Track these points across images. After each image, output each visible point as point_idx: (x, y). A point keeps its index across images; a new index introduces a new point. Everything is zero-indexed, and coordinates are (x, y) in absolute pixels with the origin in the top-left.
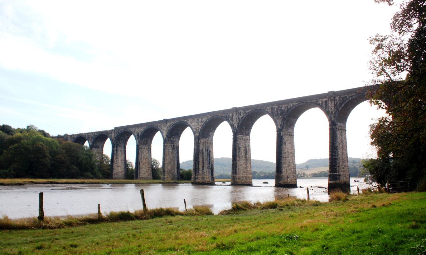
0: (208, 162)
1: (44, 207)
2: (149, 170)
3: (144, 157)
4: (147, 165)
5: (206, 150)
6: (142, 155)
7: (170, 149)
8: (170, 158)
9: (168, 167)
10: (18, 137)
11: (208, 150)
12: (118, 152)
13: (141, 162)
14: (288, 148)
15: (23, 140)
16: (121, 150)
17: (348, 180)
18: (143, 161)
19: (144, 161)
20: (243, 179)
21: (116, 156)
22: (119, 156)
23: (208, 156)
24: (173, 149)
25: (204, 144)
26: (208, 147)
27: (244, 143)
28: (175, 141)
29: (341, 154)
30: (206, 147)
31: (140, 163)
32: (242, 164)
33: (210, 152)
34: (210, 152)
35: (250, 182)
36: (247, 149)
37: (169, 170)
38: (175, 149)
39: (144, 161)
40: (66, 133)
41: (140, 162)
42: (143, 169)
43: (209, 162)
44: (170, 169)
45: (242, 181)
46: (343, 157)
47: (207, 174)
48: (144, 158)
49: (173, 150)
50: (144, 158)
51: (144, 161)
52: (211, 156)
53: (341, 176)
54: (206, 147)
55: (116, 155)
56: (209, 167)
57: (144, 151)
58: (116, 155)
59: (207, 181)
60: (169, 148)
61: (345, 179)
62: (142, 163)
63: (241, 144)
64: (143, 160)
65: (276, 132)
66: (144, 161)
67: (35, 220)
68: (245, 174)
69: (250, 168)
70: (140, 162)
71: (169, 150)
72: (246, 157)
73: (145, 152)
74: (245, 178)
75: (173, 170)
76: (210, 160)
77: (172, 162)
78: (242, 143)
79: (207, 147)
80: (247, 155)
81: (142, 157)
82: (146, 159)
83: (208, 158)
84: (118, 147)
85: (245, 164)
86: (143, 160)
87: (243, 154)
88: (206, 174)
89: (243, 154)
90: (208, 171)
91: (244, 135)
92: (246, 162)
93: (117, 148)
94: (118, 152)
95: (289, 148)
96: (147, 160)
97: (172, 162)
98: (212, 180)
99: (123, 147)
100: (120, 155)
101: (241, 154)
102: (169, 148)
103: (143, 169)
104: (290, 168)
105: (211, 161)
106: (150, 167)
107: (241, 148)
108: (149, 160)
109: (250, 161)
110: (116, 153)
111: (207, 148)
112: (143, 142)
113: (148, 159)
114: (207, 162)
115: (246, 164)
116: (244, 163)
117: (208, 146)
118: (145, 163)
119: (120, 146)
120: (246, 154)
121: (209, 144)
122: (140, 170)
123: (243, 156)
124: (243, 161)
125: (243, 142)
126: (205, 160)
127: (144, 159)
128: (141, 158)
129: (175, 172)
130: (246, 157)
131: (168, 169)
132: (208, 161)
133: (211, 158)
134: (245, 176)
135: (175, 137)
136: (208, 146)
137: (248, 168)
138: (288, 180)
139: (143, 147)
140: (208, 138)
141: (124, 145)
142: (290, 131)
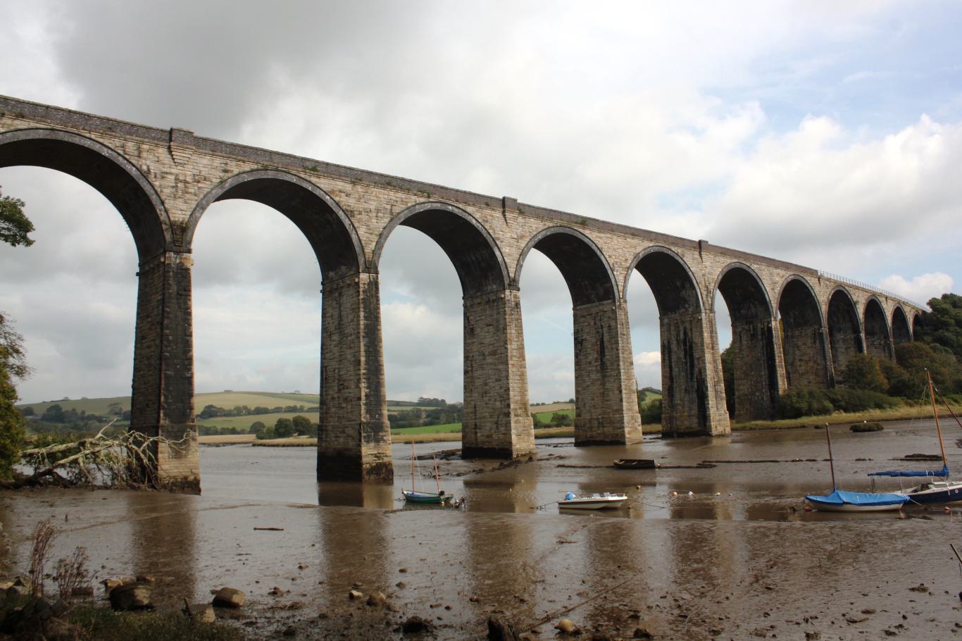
0: (687, 375)
1: (676, 466)
3: (802, 358)
5: (678, 344)
6: (794, 354)
7: (744, 338)
8: (746, 364)
9: (741, 387)
10: (28, 408)
11: (685, 340)
12: (837, 346)
13: (795, 372)
14: (482, 341)
15: (946, 316)
16: (844, 341)
17: (351, 444)
18: (798, 368)
19: (802, 369)
20: (591, 428)
23: (685, 358)
24: (753, 336)
25: (672, 328)
26: (685, 333)
27: (595, 324)
30: (678, 335)
32: (588, 386)
33: (691, 347)
34: (694, 346)
35: (617, 435)
36: (606, 338)
37: (746, 395)
38: (760, 337)
39: (803, 367)
40: (84, 396)
43: (692, 374)
44: (747, 392)
45: (589, 434)
46: (342, 373)
47: (686, 409)
49: (752, 340)
50: (801, 360)
52: (696, 355)
53: (326, 431)
54: (678, 335)
56: (692, 387)
57: (800, 343)
59: (683, 427)
60: (740, 337)
61: (341, 440)
63: (586, 330)
64: (800, 366)
65: (133, 361)
66: (803, 367)
67: (191, 478)
68: (599, 411)
69: (617, 392)
71: (741, 342)
72: (603, 363)
73: (805, 344)
74: (599, 423)
75: (757, 394)
76: (692, 366)
77: (753, 373)
78: (589, 325)
79: (682, 333)
80: (607, 357)
81: (794, 359)
82: (807, 362)
83: (686, 363)
85: (601, 384)
86: (800, 366)
87: (591, 357)
88: (683, 407)
89: (591, 357)
90: (686, 399)
91: (594, 302)
92: (604, 377)
94: (837, 346)
95: (487, 341)
96: (811, 364)
97: (751, 371)
98: (699, 423)
100: (843, 350)
101: (587, 358)
102: (740, 337)
104: (486, 399)
105: (696, 370)
107: (586, 340)
108: (818, 364)
109: (614, 373)
111: (682, 336)
112: (792, 320)
113: (815, 362)
114: (683, 374)
115: (603, 384)
116: (597, 380)
117: (685, 329)
118: (807, 372)
119: (839, 330)
120: (602, 352)
121: (688, 325)
123: (593, 362)
124: (594, 376)
125: (592, 323)
126: (675, 370)
129: (763, 398)
130: (603, 363)
131: (741, 392)
132: (686, 370)
133: (696, 362)
134: (598, 419)
135: (751, 305)
136: (685, 329)
137: (611, 393)
138: (479, 435)
139: (797, 333)
140: (684, 308)
142: (489, 288)
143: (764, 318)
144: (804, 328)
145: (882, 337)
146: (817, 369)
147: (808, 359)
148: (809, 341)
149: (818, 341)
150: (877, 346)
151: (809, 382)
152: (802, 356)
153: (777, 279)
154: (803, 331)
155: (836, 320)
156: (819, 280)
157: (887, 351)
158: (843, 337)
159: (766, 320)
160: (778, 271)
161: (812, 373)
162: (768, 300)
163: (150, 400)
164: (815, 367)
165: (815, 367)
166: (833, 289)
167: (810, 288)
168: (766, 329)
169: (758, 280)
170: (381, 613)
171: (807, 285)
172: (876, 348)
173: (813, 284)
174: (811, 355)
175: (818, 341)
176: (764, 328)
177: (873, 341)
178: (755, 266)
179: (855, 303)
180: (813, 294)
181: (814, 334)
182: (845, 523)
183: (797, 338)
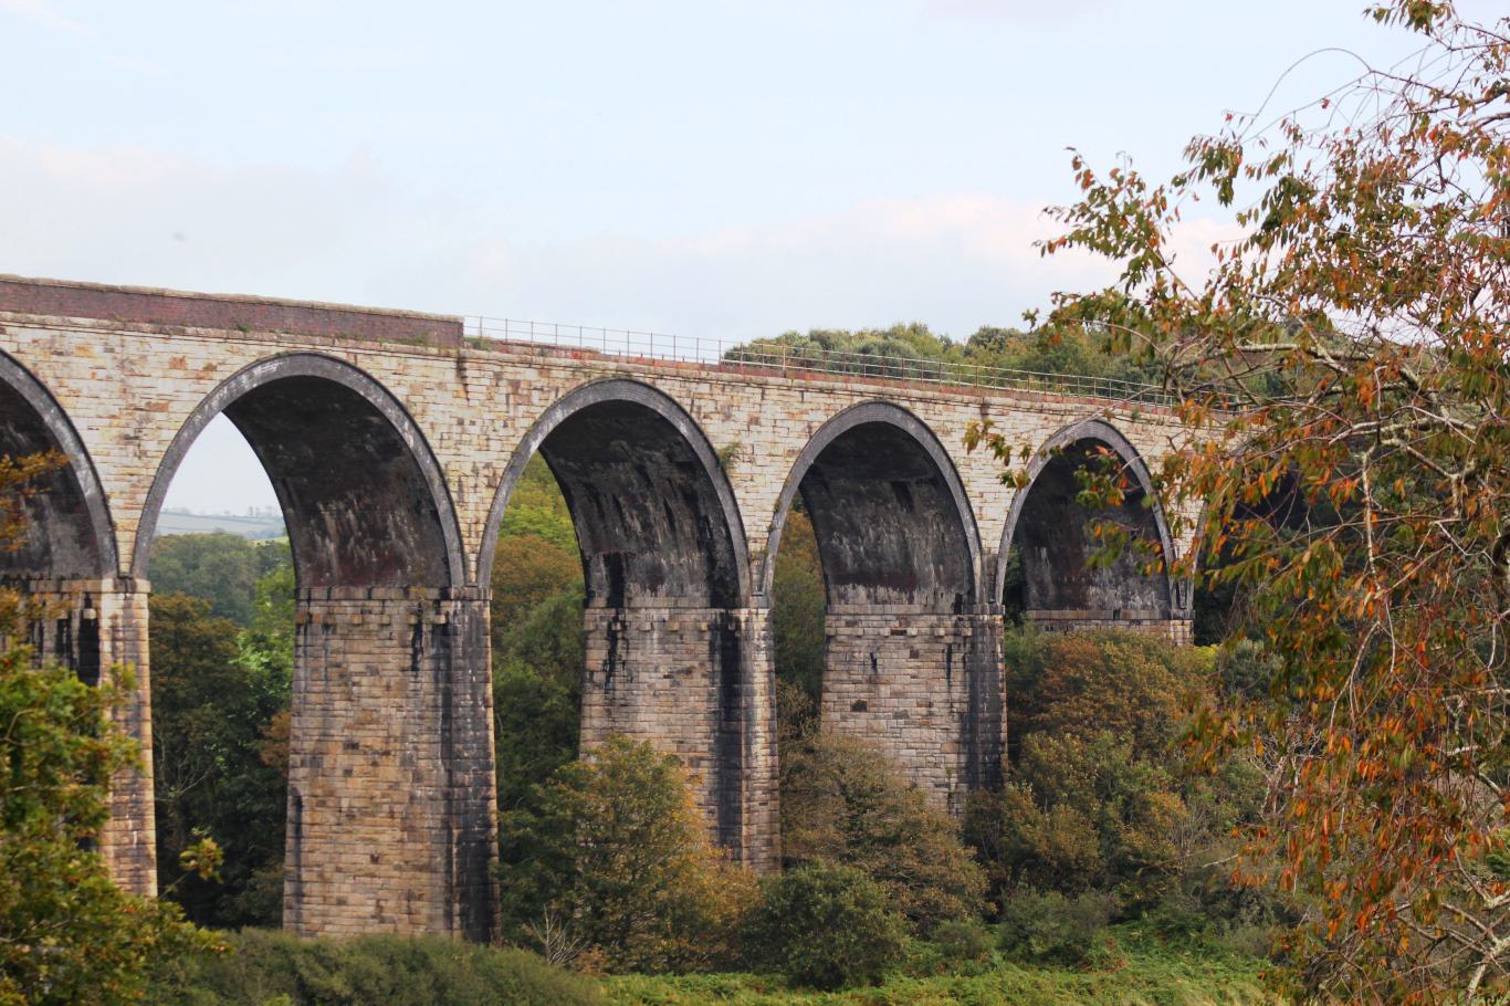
2: (410, 897)
4: (388, 836)
12: (635, 656)
16: (670, 635)
19: (351, 792)
21: (612, 705)
22: (642, 700)
28: (47, 550)
29: (259, 529)
31: (306, 817)
39: (357, 783)
41: (304, 791)
42: (343, 887)
48: (352, 746)
50: (352, 746)
51: (351, 792)
55: (607, 688)
57: (355, 664)
58: (607, 688)
62: (329, 817)
64: (348, 773)
70: (299, 804)
73: (374, 671)
81: (325, 736)
84: (633, 588)
86: (348, 773)
93: (617, 599)
94: (635, 656)
96: (390, 770)
99: (697, 593)
103: (343, 887)
106: (427, 868)
108: (418, 778)
110: (611, 663)
112: (332, 547)
113: (407, 762)
119: (654, 580)
122: (299, 895)
127: (359, 761)
128: (315, 760)
130: (447, 718)
139: (347, 611)
141: (711, 561)
143: (75, 577)
144: (379, 592)
145: (947, 601)
146: (412, 798)
147: (378, 746)
148: (395, 659)
149: (426, 665)
150: (919, 645)
151: (375, 860)
152: (360, 724)
153: (165, 387)
154: (375, 605)
155: (637, 525)
156: (460, 370)
157: (958, 675)
158: (665, 614)
159: (77, 585)
160: (178, 346)
161: (392, 814)
162: (89, 491)
163: (1117, 337)
164: (406, 787)
165: (406, 787)
166: (565, 401)
167: (392, 413)
168: (76, 624)
169: (38, 402)
170: (1309, 385)
171: (376, 399)
172: (914, 654)
173: (414, 390)
174: (396, 730)
175: (426, 665)
176: (68, 621)
177: (905, 619)
178: (26, 335)
179: (722, 462)
180: (411, 440)
181: (417, 628)
182: (1454, 486)
183: (344, 638)
